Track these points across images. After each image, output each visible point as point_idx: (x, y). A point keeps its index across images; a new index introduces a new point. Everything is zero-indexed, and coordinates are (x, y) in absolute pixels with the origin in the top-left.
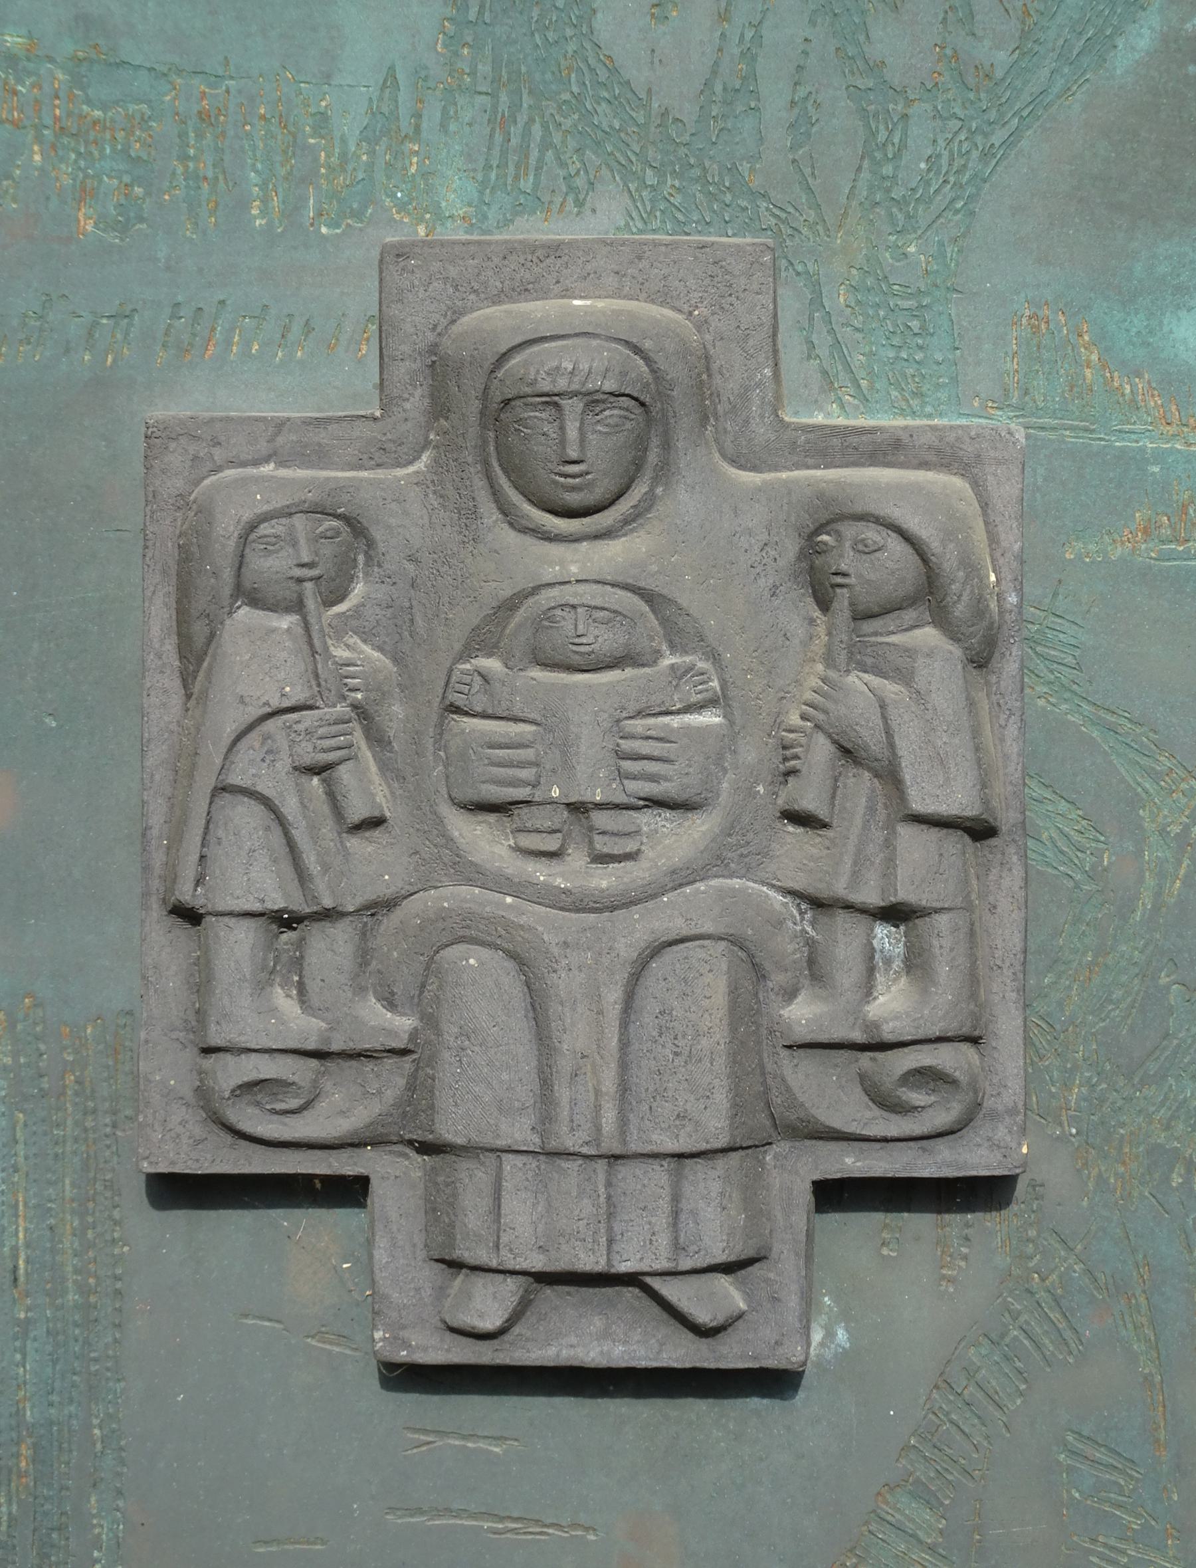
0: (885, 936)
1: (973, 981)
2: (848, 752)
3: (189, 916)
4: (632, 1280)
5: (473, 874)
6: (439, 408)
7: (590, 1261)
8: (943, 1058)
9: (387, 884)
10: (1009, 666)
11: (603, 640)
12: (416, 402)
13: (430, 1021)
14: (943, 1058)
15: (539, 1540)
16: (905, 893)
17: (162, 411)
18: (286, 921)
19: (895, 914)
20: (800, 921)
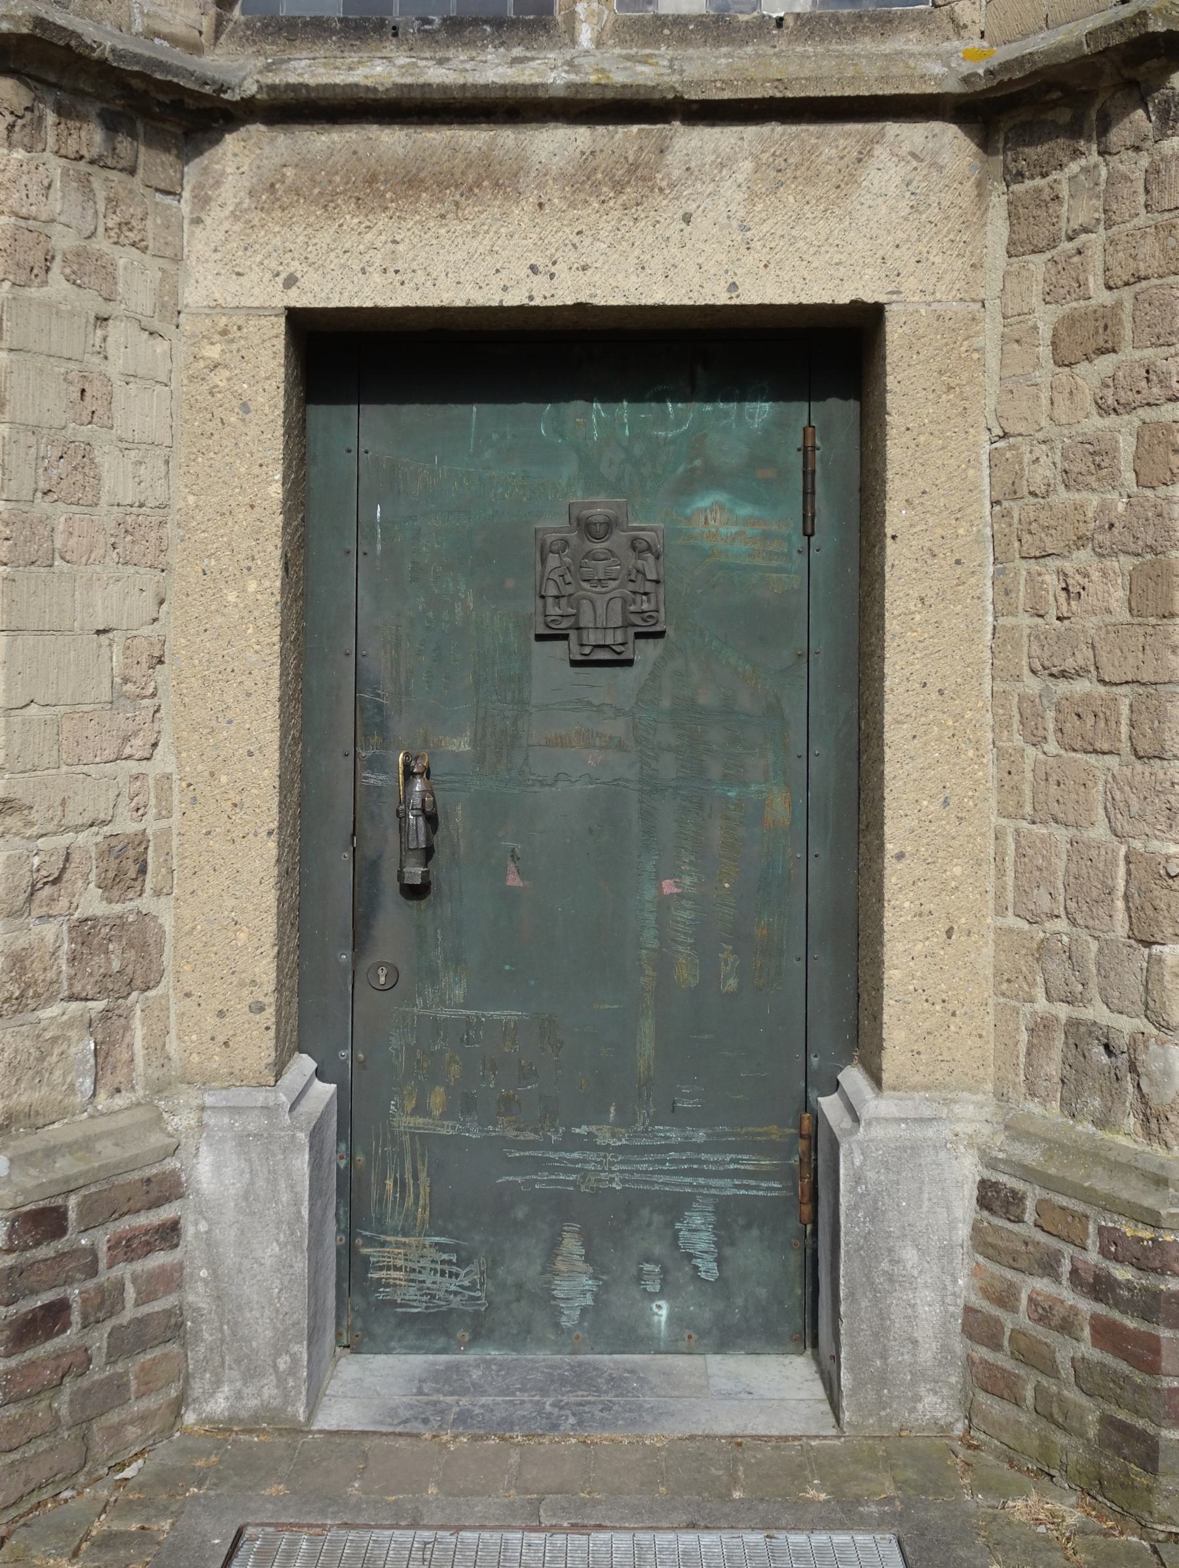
0: (644, 597)
1: (657, 603)
2: (638, 571)
3: (543, 597)
4: (608, 646)
5: (585, 590)
6: (578, 525)
7: (602, 643)
8: (653, 614)
9: (572, 591)
10: (661, 559)
11: (602, 557)
12: (575, 524)
13: (578, 610)
14: (653, 614)
15: (346, 985)
16: (647, 590)
17: (538, 526)
18: (557, 597)
19: (646, 594)
20: (632, 596)
